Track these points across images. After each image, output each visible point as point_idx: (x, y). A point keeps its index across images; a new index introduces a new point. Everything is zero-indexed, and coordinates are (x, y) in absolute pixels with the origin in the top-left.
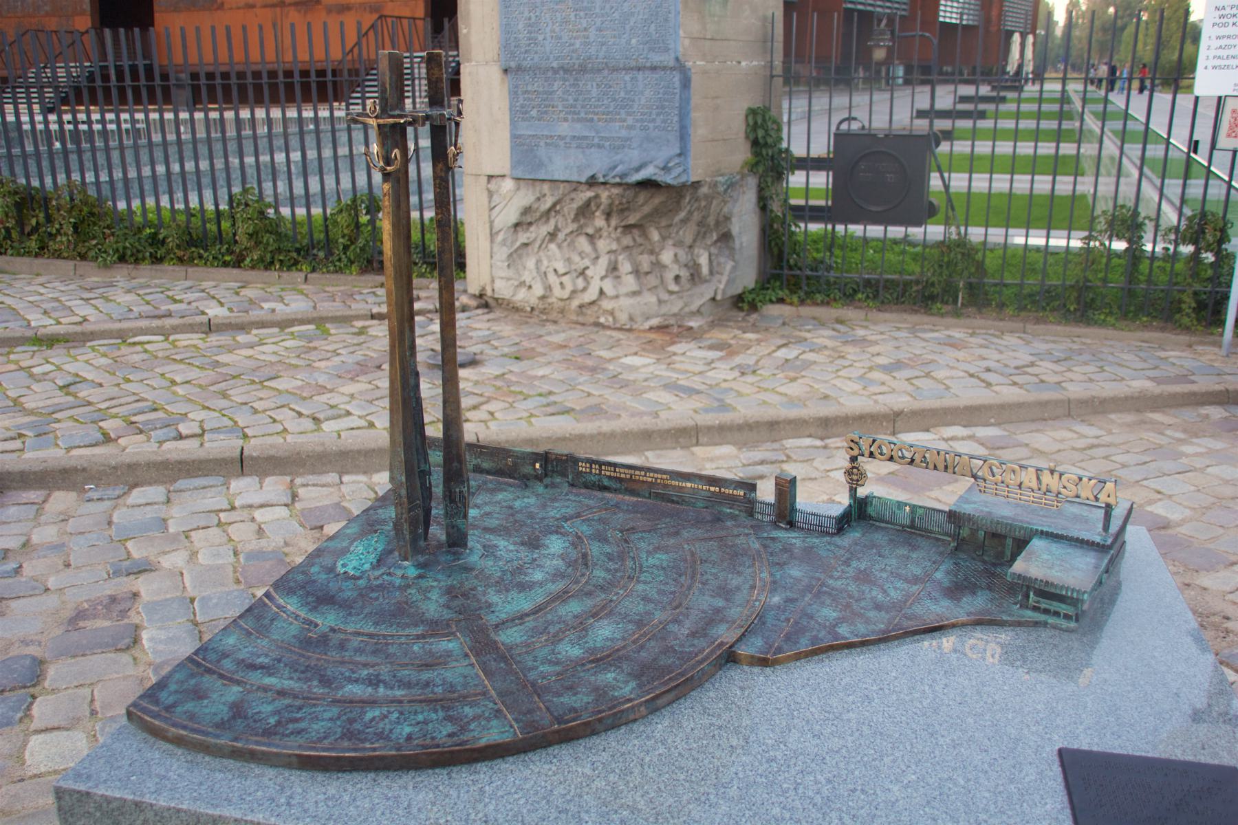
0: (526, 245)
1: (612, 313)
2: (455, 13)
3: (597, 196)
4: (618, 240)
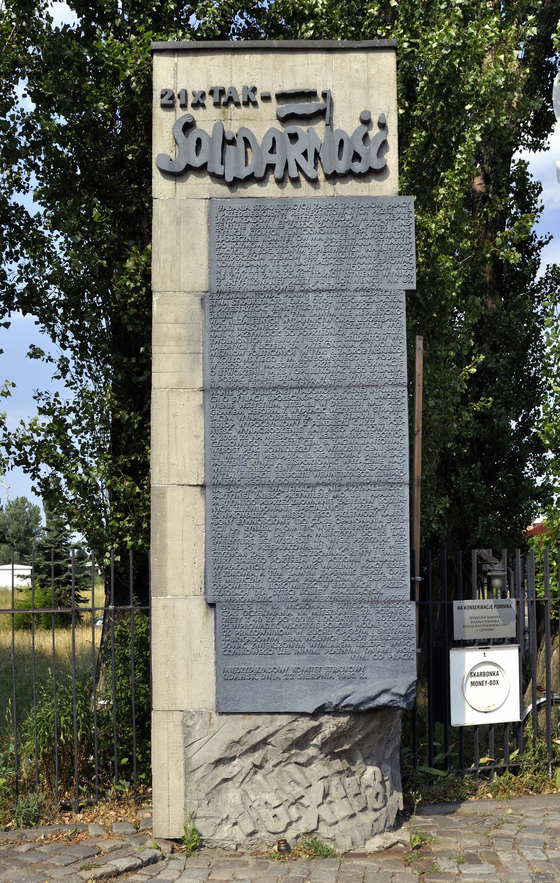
0: (226, 780)
2: (149, 238)
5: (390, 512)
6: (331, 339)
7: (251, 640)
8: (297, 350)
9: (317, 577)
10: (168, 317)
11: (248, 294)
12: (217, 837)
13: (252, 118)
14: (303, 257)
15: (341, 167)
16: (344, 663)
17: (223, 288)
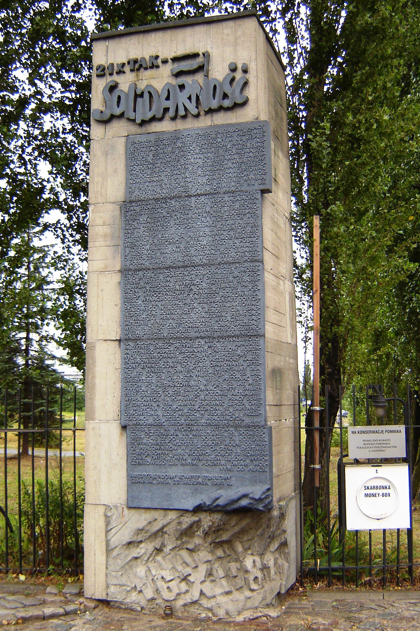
0: (136, 558)
1: (210, 610)
3: (200, 521)
4: (212, 552)
5: (249, 357)
6: (207, 230)
7: (150, 453)
8: (183, 240)
9: (196, 407)
10: (99, 221)
11: (150, 202)
12: (128, 600)
13: (155, 77)
14: (187, 172)
15: (214, 104)
16: (215, 473)
17: (133, 198)
